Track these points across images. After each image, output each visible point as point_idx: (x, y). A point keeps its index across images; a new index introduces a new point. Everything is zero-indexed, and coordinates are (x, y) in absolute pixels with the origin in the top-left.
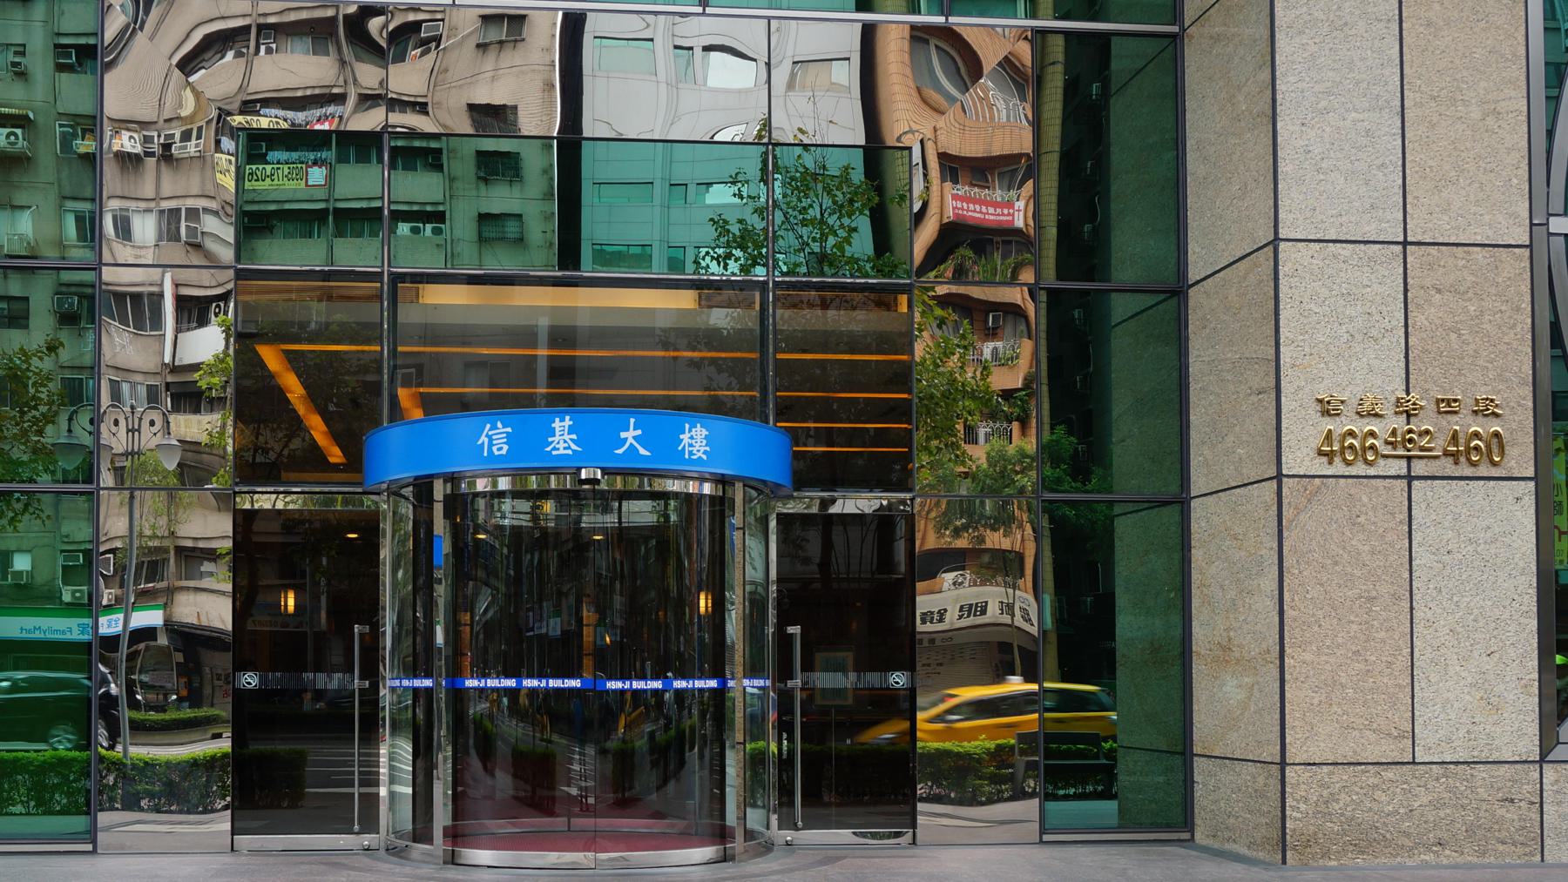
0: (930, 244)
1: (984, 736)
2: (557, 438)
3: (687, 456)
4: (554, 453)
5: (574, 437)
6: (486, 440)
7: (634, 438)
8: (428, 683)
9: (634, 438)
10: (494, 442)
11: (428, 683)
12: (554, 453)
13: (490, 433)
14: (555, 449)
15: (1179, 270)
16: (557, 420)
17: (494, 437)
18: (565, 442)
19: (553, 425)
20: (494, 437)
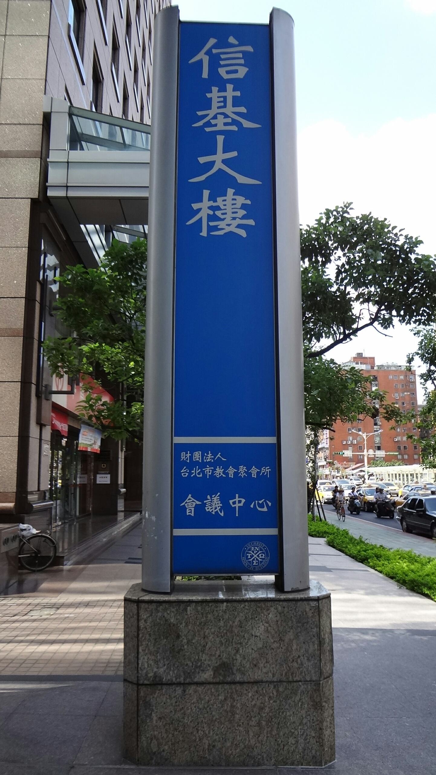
0: (149, 220)
1: (270, 504)
2: (211, 113)
3: (204, 233)
4: (208, 130)
5: (243, 110)
6: (206, 60)
7: (224, 162)
8: (19, 556)
9: (224, 162)
10: (222, 63)
11: (19, 556)
12: (208, 130)
13: (214, 51)
14: (208, 124)
15: (85, 549)
16: (215, 89)
17: (223, 56)
18: (226, 116)
19: (209, 95)
20: (223, 56)
